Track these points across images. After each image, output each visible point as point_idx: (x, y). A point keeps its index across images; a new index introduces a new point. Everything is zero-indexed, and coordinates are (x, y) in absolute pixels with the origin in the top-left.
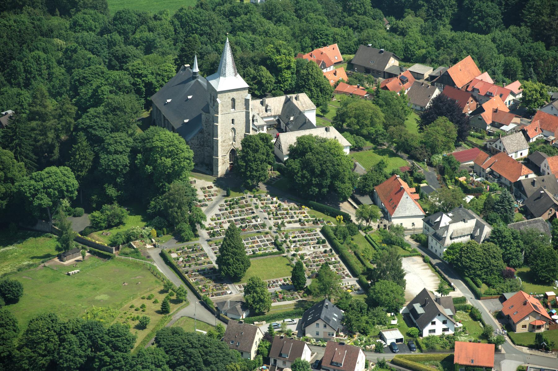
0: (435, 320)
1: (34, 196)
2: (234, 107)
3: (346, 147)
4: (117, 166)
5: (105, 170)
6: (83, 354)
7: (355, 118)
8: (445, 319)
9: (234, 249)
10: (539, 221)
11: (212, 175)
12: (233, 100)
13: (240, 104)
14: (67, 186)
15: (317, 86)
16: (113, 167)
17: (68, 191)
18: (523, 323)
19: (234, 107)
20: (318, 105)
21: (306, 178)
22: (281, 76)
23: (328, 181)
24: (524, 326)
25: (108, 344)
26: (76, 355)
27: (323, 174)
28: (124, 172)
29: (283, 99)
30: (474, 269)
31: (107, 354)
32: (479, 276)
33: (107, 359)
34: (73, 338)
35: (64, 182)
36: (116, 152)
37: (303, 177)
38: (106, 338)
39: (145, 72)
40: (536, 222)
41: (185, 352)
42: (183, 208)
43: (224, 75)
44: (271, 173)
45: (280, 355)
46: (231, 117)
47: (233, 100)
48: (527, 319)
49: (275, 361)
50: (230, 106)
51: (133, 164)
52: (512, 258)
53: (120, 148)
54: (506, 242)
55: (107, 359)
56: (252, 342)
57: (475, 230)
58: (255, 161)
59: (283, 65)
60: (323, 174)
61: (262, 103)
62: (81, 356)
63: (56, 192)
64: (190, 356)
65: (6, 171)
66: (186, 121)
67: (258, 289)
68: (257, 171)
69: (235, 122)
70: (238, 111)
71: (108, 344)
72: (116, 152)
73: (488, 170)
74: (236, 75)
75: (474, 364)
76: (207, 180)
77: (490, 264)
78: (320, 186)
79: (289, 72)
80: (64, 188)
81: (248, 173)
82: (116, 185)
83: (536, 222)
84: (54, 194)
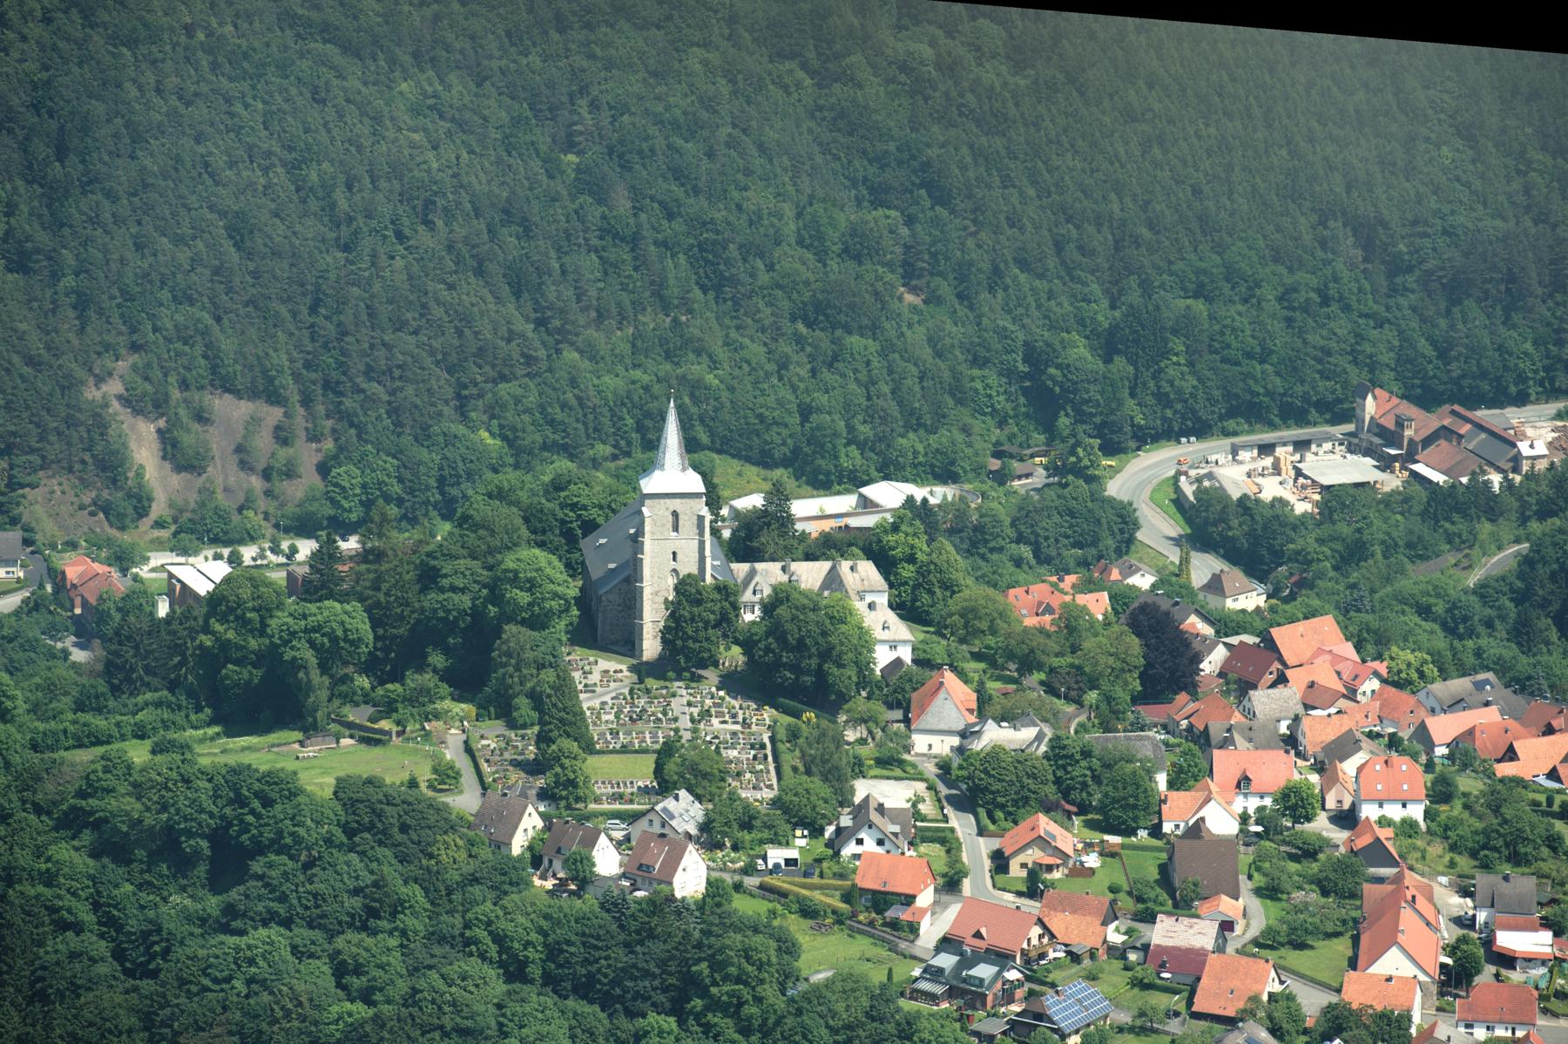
0: (862, 835)
1: (286, 643)
2: (676, 528)
3: (905, 642)
4: (449, 612)
5: (429, 619)
6: (215, 810)
7: (961, 616)
8: (881, 836)
9: (562, 714)
10: (1148, 738)
11: (632, 656)
12: (675, 514)
13: (688, 524)
14: (345, 631)
15: (947, 588)
16: (441, 614)
17: (346, 640)
18: (1021, 858)
19: (676, 528)
20: (891, 585)
21: (773, 651)
22: (897, 574)
23: (814, 662)
24: (1024, 865)
25: (256, 795)
26: (202, 811)
27: (801, 645)
28: (462, 625)
29: (826, 566)
30: (993, 793)
31: (253, 812)
32: (1002, 807)
33: (250, 818)
34: (203, 784)
35: (343, 623)
36: (454, 589)
37: (768, 650)
38: (257, 786)
39: (585, 501)
40: (1141, 739)
41: (374, 811)
42: (525, 671)
43: (662, 467)
44: (734, 656)
45: (559, 851)
46: (670, 547)
47: (675, 514)
48: (1030, 852)
49: (551, 862)
50: (670, 526)
51: (474, 607)
52: (1074, 789)
53: (460, 582)
54: (1065, 757)
55: (250, 818)
56: (516, 828)
57: (1031, 744)
58: (693, 619)
59: (897, 553)
60: (801, 645)
61: (784, 569)
62: (211, 815)
63: (326, 640)
64: (379, 816)
65: (263, 612)
66: (612, 566)
67: (567, 762)
68: (696, 640)
69: (679, 557)
70: (673, 523)
71: (256, 795)
72: (454, 589)
73: (1184, 723)
74: (684, 469)
75: (888, 888)
76: (620, 662)
77: (1023, 787)
78: (795, 668)
79: (911, 567)
80: (340, 633)
81: (679, 643)
82: (447, 651)
83: (1141, 739)
84: (323, 644)
